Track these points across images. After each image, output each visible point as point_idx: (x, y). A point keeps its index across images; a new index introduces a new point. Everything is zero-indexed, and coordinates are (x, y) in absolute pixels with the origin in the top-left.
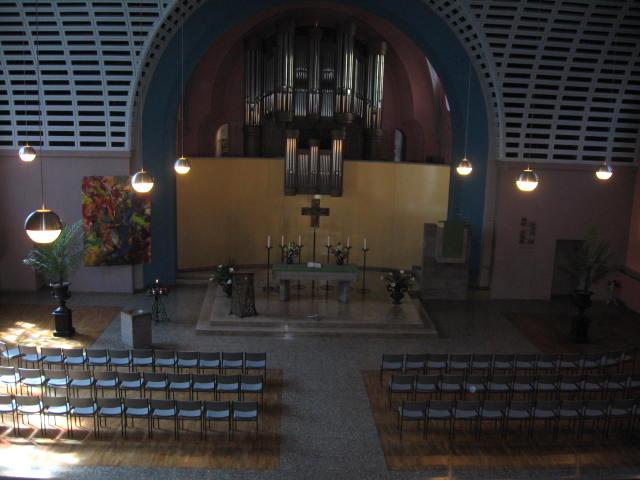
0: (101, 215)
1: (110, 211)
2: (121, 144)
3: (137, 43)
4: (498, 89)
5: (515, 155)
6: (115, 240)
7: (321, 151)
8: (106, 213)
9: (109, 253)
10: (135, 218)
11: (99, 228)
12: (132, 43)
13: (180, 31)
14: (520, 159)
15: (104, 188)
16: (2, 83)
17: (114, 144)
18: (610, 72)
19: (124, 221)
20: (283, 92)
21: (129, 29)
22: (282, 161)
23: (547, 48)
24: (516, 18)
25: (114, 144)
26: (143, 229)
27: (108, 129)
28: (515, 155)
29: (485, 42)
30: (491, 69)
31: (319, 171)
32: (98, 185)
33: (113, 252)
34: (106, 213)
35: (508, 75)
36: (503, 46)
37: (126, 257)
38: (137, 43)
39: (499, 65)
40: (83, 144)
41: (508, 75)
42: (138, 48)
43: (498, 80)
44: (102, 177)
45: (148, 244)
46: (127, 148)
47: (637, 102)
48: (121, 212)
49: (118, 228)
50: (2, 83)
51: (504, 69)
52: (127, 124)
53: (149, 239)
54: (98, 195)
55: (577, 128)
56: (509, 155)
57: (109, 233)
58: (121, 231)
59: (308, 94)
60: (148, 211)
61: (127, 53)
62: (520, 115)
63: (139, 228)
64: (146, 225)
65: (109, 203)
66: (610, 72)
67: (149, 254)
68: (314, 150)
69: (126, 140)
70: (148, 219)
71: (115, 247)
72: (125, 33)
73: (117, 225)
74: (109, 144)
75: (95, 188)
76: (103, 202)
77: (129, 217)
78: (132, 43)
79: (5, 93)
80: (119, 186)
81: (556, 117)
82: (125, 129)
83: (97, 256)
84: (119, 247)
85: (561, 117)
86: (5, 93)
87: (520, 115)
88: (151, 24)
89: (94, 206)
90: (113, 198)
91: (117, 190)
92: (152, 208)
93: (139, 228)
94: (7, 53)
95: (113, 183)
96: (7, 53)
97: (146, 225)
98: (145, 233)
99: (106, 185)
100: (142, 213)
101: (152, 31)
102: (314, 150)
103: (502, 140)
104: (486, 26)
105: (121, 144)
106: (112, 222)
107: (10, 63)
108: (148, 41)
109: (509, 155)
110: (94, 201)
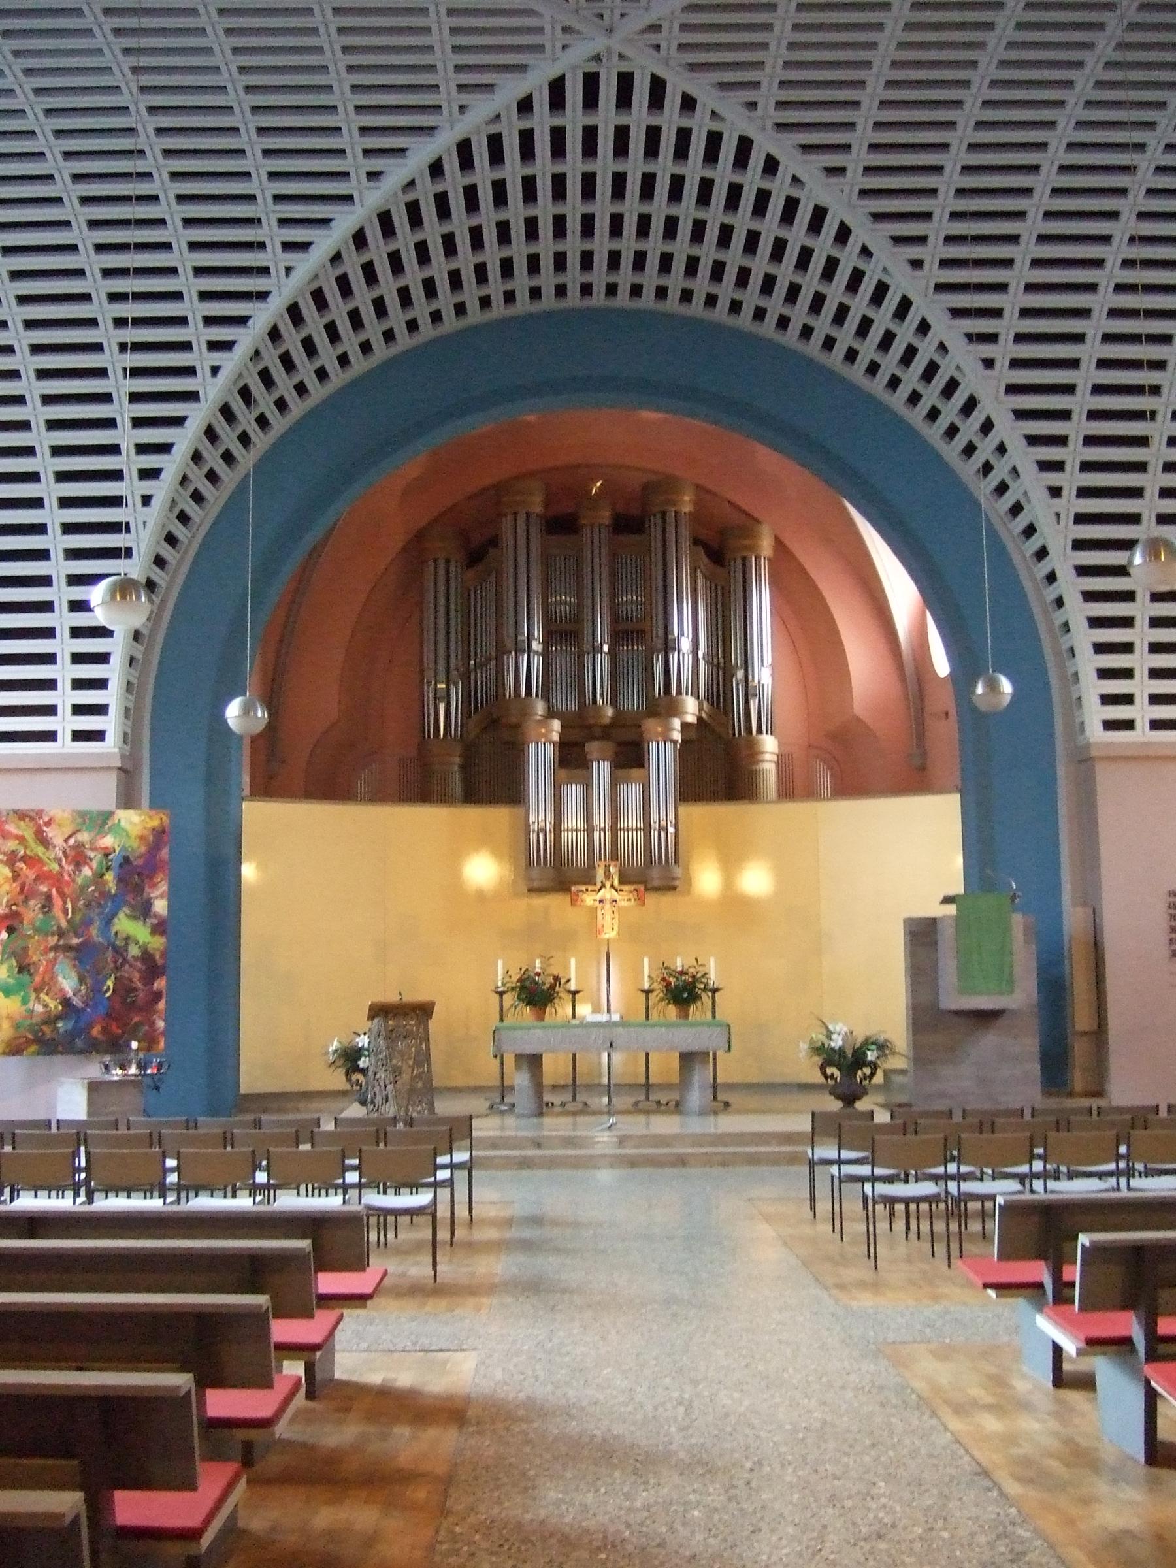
0: (32, 913)
1: (57, 901)
2: (98, 736)
3: (214, 346)
4: (1063, 560)
5: (1129, 725)
6: (68, 982)
7: (621, 773)
8: (47, 905)
9: (50, 1020)
10: (125, 924)
11: (25, 949)
12: (131, 474)
13: (242, 488)
14: (1142, 734)
15: (45, 842)
16: (1, 325)
17: (78, 736)
18: (1132, 313)
19: (94, 931)
20: (518, 651)
21: (126, 437)
22: (519, 811)
23: (1008, 263)
24: (1155, 442)
25: (78, 736)
26: (147, 956)
27: (64, 697)
28: (1129, 725)
29: (1009, 431)
30: (1039, 509)
31: (647, 1078)
32: (29, 835)
33: (59, 1017)
34: (47, 905)
35: (1082, 519)
36: (1062, 441)
37: (96, 1031)
38: (214, 346)
39: (1055, 492)
40: (1156, 725)
41: (1082, 519)
42: (148, 487)
43: (1058, 535)
44: (40, 813)
45: (158, 996)
46: (111, 745)
47: (1171, 85)
48: (88, 905)
49: (77, 949)
50: (1, 325)
51: (1073, 504)
52: (113, 685)
53: (160, 984)
54: (28, 860)
55: (1136, 493)
56: (1109, 725)
57: (53, 962)
58: (84, 955)
59: (580, 656)
60: (160, 906)
61: (190, 371)
62: (1127, 622)
63: (134, 951)
64: (157, 943)
65: (57, 880)
66: (1132, 313)
67: (161, 1024)
68: (601, 771)
69: (110, 724)
70: (159, 928)
71: (66, 1002)
72: (182, 321)
73: (75, 941)
74: (1142, 725)
75: (21, 839)
76: (38, 878)
77: (109, 922)
78: (131, 474)
79: (9, 350)
80: (84, 837)
81: (1075, 441)
82: (110, 697)
83: (17, 1026)
84: (77, 1002)
85: (1087, 466)
86: (9, 350)
87: (1127, 622)
88: (179, 421)
89: (16, 886)
90: (69, 868)
91: (79, 846)
92: (172, 897)
93: (134, 951)
94: (16, 275)
95: (68, 831)
96: (16, 275)
97: (157, 943)
98: (152, 967)
99: (50, 832)
100: (144, 910)
101: (184, 439)
102: (601, 771)
103: (1092, 688)
104: (1012, 389)
105: (98, 736)
106: (61, 934)
107: (23, 300)
108: (172, 465)
109: (1109, 725)
110: (16, 876)
